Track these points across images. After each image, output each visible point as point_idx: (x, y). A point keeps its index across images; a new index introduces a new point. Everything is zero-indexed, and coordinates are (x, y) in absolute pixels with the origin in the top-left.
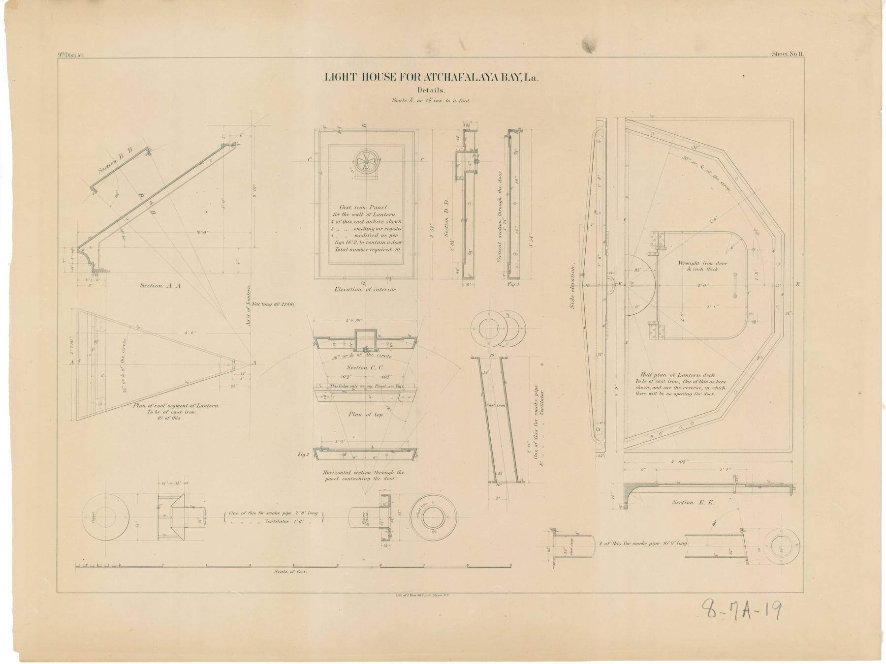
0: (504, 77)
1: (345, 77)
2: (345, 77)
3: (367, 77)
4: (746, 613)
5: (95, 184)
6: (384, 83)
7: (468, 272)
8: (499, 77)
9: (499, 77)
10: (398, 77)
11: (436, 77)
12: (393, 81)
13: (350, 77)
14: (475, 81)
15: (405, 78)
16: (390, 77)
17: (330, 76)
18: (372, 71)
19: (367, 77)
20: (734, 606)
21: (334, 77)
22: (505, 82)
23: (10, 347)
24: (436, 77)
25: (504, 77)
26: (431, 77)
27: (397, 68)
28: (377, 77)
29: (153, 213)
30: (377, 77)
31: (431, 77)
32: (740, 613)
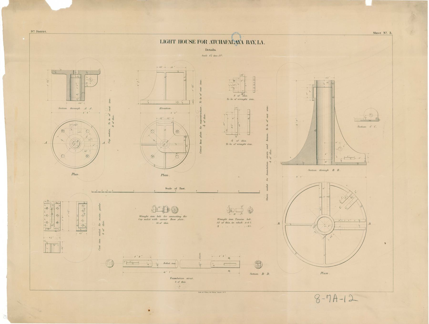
2: (170, 42)
8: (245, 42)
9: (245, 42)
12: (194, 44)
13: (173, 42)
14: (233, 45)
15: (200, 43)
17: (162, 41)
18: (184, 39)
22: (248, 45)
25: (248, 42)
27: (177, 38)
28: (186, 42)
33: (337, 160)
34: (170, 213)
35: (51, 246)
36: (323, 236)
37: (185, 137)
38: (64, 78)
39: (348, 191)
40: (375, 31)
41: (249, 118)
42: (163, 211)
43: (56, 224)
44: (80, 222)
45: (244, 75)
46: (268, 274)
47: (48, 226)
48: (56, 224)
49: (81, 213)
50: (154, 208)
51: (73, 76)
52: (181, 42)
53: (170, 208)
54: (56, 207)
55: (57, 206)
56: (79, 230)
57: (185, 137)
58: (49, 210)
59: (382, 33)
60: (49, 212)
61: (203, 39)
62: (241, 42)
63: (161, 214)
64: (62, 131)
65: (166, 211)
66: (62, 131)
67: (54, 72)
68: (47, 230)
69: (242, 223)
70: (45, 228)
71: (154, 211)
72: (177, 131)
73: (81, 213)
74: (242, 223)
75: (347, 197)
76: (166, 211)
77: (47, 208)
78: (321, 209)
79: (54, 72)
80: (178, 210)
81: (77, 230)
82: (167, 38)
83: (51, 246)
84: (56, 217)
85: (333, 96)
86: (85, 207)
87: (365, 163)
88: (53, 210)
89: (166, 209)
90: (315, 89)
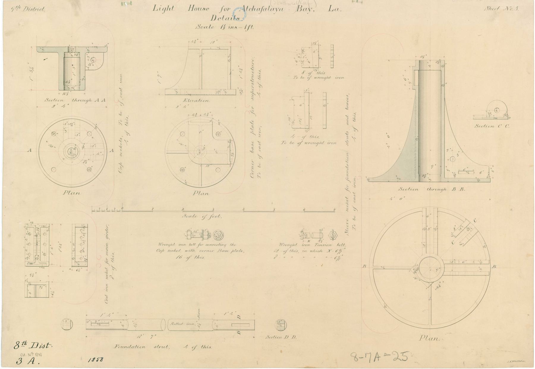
33: (449, 175)
34: (212, 240)
35: (35, 288)
36: (428, 285)
37: (230, 142)
38: (55, 59)
39: (464, 220)
41: (325, 106)
42: (202, 237)
43: (42, 256)
44: (78, 253)
45: (317, 43)
47: (31, 259)
48: (42, 256)
49: (78, 241)
50: (189, 233)
51: (68, 55)
53: (212, 232)
54: (42, 232)
55: (43, 230)
56: (77, 265)
57: (230, 142)
58: (32, 236)
60: (31, 239)
63: (199, 240)
64: (53, 133)
65: (205, 237)
66: (53, 133)
67: (42, 50)
68: (29, 265)
69: (321, 251)
70: (26, 263)
71: (189, 237)
72: (218, 134)
73: (78, 241)
74: (321, 251)
75: (463, 229)
76: (205, 237)
77: (29, 234)
78: (425, 246)
79: (42, 50)
80: (223, 235)
81: (74, 265)
83: (35, 288)
84: (42, 245)
85: (443, 83)
86: (86, 231)
87: (489, 180)
88: (39, 237)
89: (206, 234)
90: (417, 72)
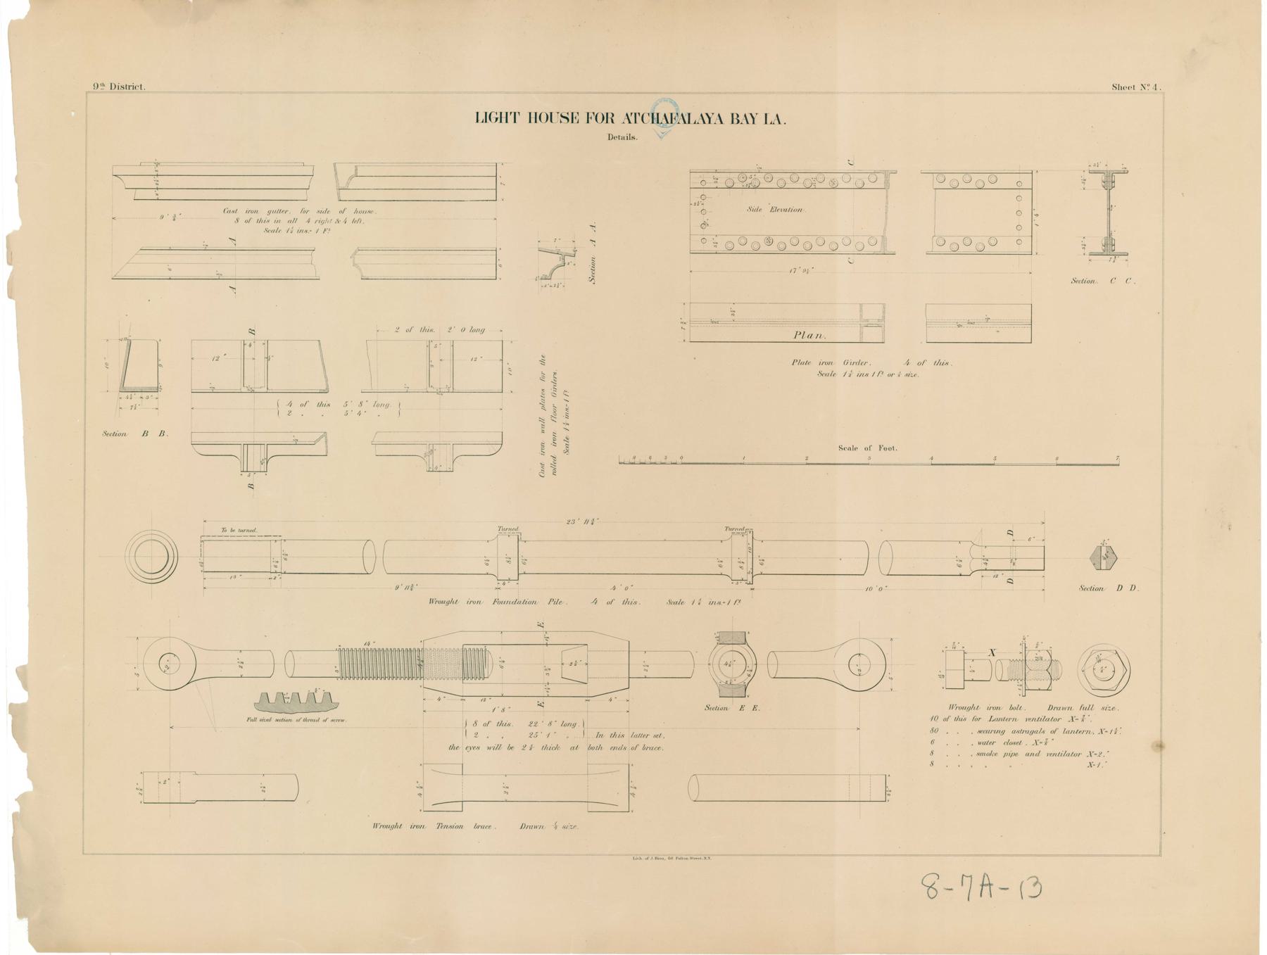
0: (706, 119)
1: (502, 118)
2: (502, 118)
3: (535, 118)
4: (986, 889)
5: (884, 331)
6: (558, 127)
7: (140, 376)
8: (727, 118)
9: (727, 118)
10: (583, 118)
11: (639, 118)
13: (511, 118)
14: (691, 125)
15: (592, 121)
16: (570, 118)
17: (482, 117)
18: (544, 109)
19: (535, 118)
20: (967, 880)
21: (488, 117)
23: (29, 508)
24: (639, 118)
25: (735, 119)
26: (632, 119)
27: (580, 106)
28: (550, 117)
29: (252, 331)
30: (550, 117)
31: (632, 119)
32: (976, 888)
40: (1116, 82)
46: (162, 433)
52: (538, 117)
59: (1138, 87)
61: (602, 110)
62: (714, 119)
82: (495, 107)
